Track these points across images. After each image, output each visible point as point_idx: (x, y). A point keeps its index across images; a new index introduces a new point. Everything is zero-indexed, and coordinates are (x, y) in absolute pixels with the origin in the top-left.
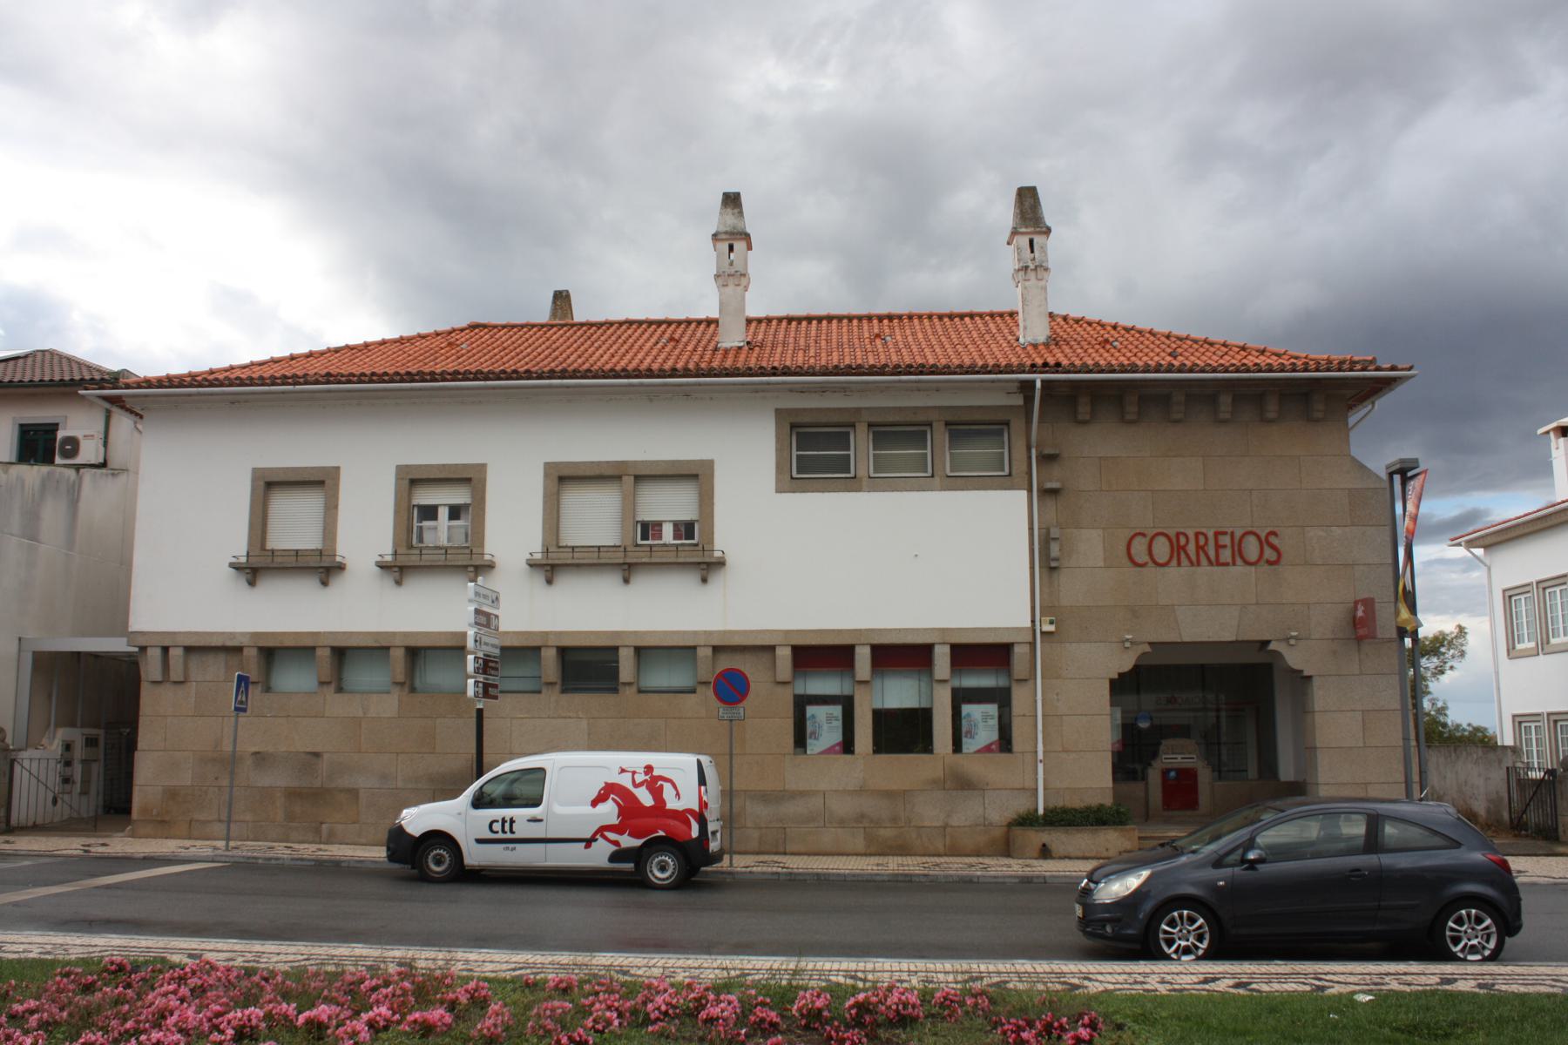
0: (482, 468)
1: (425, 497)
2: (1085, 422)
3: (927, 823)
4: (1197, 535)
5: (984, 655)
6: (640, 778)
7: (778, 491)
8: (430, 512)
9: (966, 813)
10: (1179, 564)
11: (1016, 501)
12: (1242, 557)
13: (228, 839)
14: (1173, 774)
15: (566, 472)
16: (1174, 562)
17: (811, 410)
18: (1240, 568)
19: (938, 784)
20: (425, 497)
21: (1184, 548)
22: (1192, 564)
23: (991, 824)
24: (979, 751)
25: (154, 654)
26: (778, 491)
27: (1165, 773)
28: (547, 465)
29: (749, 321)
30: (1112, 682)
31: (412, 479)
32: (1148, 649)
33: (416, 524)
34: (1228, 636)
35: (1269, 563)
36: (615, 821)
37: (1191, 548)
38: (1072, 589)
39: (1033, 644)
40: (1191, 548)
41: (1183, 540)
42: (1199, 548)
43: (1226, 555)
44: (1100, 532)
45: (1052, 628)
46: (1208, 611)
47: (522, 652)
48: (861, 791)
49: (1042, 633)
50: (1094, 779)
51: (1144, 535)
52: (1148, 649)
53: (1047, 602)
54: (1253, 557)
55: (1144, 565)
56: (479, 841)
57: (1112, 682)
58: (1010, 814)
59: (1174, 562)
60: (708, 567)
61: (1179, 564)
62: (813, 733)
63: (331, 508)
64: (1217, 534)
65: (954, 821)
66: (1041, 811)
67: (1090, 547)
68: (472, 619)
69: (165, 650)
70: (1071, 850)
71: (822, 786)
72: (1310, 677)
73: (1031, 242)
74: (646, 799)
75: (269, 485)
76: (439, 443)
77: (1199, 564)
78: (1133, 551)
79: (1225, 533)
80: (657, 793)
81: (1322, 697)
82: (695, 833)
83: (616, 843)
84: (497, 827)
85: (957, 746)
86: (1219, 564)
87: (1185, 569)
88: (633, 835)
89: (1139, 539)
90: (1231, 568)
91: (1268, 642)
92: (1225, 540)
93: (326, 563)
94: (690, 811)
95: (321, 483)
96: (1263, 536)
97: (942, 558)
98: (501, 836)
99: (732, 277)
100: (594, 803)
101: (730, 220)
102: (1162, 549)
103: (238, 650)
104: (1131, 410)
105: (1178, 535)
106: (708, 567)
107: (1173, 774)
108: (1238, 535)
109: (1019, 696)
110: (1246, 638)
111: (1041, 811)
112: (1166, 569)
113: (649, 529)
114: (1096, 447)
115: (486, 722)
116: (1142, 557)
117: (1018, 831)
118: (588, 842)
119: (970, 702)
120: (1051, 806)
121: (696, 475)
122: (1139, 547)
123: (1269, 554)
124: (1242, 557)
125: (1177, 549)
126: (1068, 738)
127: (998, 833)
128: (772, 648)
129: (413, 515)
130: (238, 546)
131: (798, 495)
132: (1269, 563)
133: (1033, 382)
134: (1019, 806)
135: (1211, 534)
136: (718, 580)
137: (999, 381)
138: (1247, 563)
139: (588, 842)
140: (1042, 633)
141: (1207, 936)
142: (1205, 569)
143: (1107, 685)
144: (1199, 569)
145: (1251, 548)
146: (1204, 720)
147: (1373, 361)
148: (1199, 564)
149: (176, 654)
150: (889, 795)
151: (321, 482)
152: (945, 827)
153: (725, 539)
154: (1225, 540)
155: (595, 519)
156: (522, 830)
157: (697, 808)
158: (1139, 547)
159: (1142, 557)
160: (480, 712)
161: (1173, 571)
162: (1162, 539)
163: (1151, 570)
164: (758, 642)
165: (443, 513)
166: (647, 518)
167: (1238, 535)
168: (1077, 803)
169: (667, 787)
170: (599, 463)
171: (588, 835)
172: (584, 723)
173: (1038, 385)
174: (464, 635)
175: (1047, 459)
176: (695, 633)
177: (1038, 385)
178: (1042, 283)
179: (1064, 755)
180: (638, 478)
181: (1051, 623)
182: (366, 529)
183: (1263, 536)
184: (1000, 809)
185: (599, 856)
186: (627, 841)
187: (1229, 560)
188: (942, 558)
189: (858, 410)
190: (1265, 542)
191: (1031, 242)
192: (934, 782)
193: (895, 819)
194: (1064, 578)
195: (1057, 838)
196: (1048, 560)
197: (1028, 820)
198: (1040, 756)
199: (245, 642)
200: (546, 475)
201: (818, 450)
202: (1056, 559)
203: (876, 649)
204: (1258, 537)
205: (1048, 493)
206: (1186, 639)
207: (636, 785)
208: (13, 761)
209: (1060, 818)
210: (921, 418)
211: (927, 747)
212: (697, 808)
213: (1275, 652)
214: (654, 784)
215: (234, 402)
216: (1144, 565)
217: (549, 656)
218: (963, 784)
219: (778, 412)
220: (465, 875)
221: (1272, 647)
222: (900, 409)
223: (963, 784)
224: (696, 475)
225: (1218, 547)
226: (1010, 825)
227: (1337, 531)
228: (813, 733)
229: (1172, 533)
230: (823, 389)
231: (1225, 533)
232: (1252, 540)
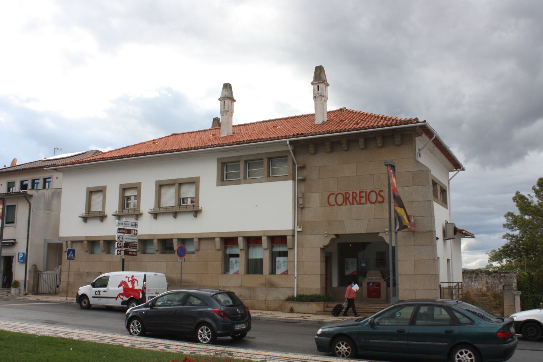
0: (140, 184)
1: (128, 193)
2: (399, 145)
3: (260, 299)
4: (353, 193)
5: (277, 240)
6: (130, 279)
7: (217, 186)
8: (129, 198)
9: (274, 295)
10: (346, 205)
11: (289, 184)
12: (369, 201)
13: (67, 297)
14: (371, 284)
15: (161, 184)
16: (345, 203)
17: (266, 153)
18: (369, 205)
19: (263, 285)
20: (128, 193)
21: (348, 198)
22: (351, 204)
24: (281, 274)
25: (64, 243)
26: (217, 186)
27: (369, 283)
28: (157, 182)
29: (233, 126)
31: (124, 189)
32: (334, 237)
33: (126, 202)
34: (363, 231)
35: (380, 202)
36: (122, 292)
38: (309, 215)
39: (293, 236)
41: (348, 195)
42: (354, 198)
43: (363, 200)
44: (319, 194)
45: (300, 230)
46: (358, 221)
47: (145, 243)
48: (241, 287)
49: (298, 232)
50: (314, 284)
51: (334, 194)
52: (334, 237)
53: (299, 220)
55: (333, 205)
56: (93, 297)
57: (321, 249)
58: (286, 297)
59: (345, 203)
60: (196, 212)
61: (346, 205)
62: (278, 267)
63: (104, 198)
64: (360, 192)
65: (268, 299)
66: (295, 296)
67: (315, 199)
68: (117, 231)
69: (67, 242)
70: (300, 310)
71: (229, 285)
73: (318, 86)
74: (130, 286)
75: (91, 192)
76: (129, 177)
77: (353, 204)
78: (330, 200)
79: (363, 192)
80: (133, 283)
81: (401, 255)
82: (141, 297)
83: (122, 299)
84: (97, 293)
85: (273, 271)
86: (361, 204)
87: (348, 206)
88: (127, 297)
89: (332, 196)
91: (379, 233)
92: (363, 194)
93: (101, 215)
94: (140, 290)
95: (102, 191)
97: (265, 206)
98: (97, 296)
99: (319, 97)
100: (119, 287)
101: (227, 94)
102: (340, 199)
103: (82, 242)
104: (398, 140)
105: (346, 193)
106: (196, 212)
107: (371, 284)
110: (370, 232)
111: (295, 296)
112: (341, 206)
113: (184, 200)
114: (320, 162)
115: (125, 263)
116: (333, 203)
118: (116, 298)
119: (280, 256)
120: (299, 294)
121: (194, 182)
122: (332, 198)
123: (380, 199)
124: (369, 201)
126: (304, 270)
128: (214, 238)
129: (124, 201)
130: (82, 210)
131: (231, 186)
132: (380, 202)
133: (286, 141)
134: (288, 294)
135: (358, 193)
136: (200, 216)
137: (281, 142)
138: (371, 203)
139: (116, 298)
140: (298, 232)
141: (460, 351)
142: (356, 206)
143: (319, 250)
145: (373, 197)
146: (358, 262)
147: (417, 119)
148: (353, 204)
149: (69, 243)
150: (249, 288)
151: (101, 190)
152: (266, 300)
153: (202, 204)
154: (363, 194)
155: (169, 198)
156: (103, 294)
157: (142, 289)
159: (333, 203)
160: (123, 260)
161: (344, 207)
162: (340, 195)
163: (336, 207)
164: (210, 237)
165: (132, 198)
166: (183, 197)
167: (368, 192)
168: (308, 293)
169: (136, 282)
170: (169, 180)
171: (116, 296)
172: (165, 264)
173: (288, 142)
174: (115, 236)
175: (301, 168)
176: (193, 234)
180: (180, 184)
181: (300, 228)
182: (112, 205)
183: (377, 192)
184: (283, 295)
185: (118, 303)
186: (125, 299)
187: (365, 202)
188: (265, 206)
189: (241, 156)
191: (318, 86)
192: (263, 284)
193: (250, 297)
194: (306, 211)
195: (296, 306)
196: (300, 205)
197: (291, 299)
198: (296, 276)
199: (84, 239)
200: (156, 185)
201: (228, 172)
203: (221, 238)
204: (375, 192)
206: (348, 233)
207: (129, 281)
208: (39, 274)
209: (301, 299)
210: (260, 157)
211: (261, 273)
212: (142, 289)
214: (133, 281)
215: (82, 168)
216: (333, 205)
217: (218, 240)
218: (272, 285)
219: (218, 159)
220: (89, 307)
221: (380, 235)
222: (253, 155)
223: (272, 285)
224: (194, 182)
225: (361, 197)
227: (407, 189)
228: (278, 267)
229: (344, 193)
230: (228, 150)
231: (363, 192)
232: (373, 193)
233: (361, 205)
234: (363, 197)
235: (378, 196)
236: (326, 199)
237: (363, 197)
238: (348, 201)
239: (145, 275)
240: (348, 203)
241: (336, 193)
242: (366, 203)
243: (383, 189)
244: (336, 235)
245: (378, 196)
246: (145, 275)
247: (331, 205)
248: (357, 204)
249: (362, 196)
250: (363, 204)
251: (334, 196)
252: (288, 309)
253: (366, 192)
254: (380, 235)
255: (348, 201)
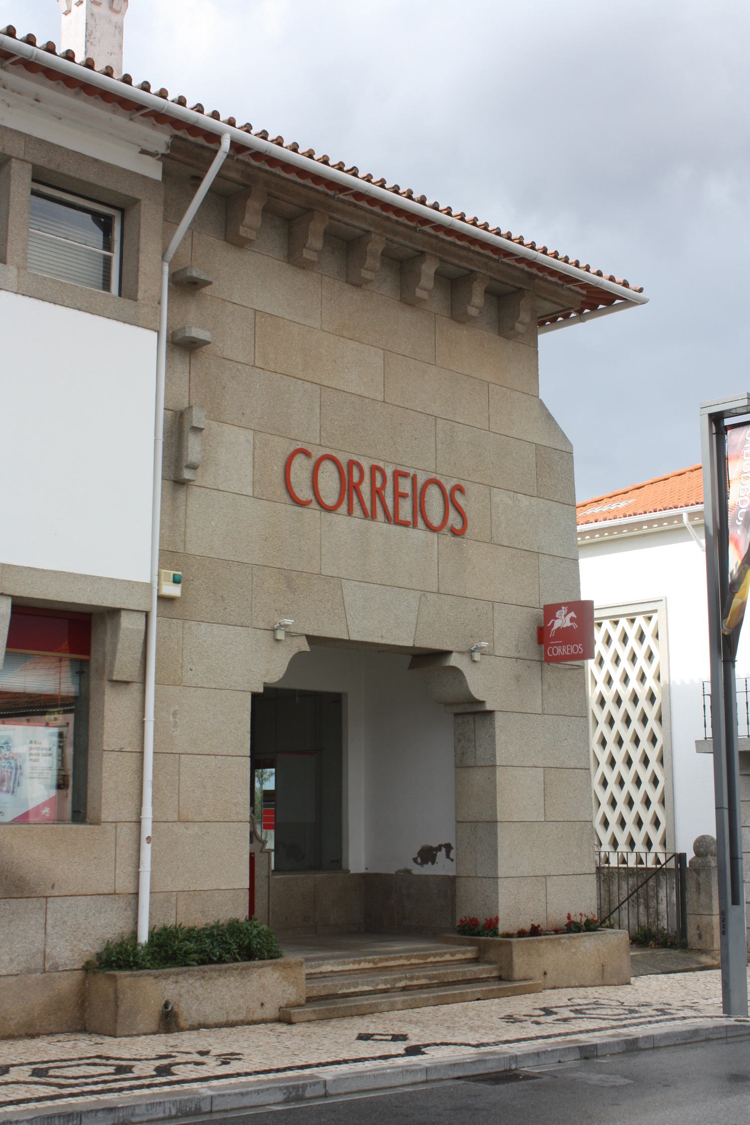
10: (350, 512)
12: (424, 517)
16: (344, 508)
18: (419, 534)
23: (55, 968)
30: (255, 696)
32: (306, 647)
35: (455, 533)
37: (365, 488)
40: (365, 488)
42: (376, 492)
43: (406, 509)
44: (250, 435)
51: (307, 454)
54: (436, 519)
57: (255, 696)
58: (89, 947)
59: (344, 508)
61: (350, 512)
64: (397, 474)
72: (491, 712)
77: (374, 517)
79: (405, 475)
87: (357, 522)
90: (410, 531)
91: (449, 653)
92: (405, 486)
96: (448, 488)
108: (421, 481)
109: (114, 712)
111: (143, 937)
114: (256, 288)
116: (305, 494)
117: (101, 984)
122: (301, 470)
123: (454, 519)
124: (424, 517)
125: (349, 488)
127: (66, 984)
134: (102, 927)
135: (389, 472)
142: (379, 526)
144: (372, 524)
148: (374, 517)
154: (405, 486)
158: (301, 470)
159: (305, 494)
161: (340, 519)
163: (313, 513)
167: (421, 481)
173: (226, 144)
177: (226, 144)
178: (115, 18)
179: (180, 828)
181: (176, 581)
183: (448, 488)
184: (73, 934)
187: (409, 518)
190: (449, 501)
194: (195, 501)
197: (118, 958)
202: (193, 467)
205: (182, 346)
206: (355, 637)
209: (174, 949)
213: (455, 669)
225: (398, 495)
226: (88, 968)
227: (524, 501)
229: (343, 459)
231: (405, 475)
232: (433, 491)
233: (394, 528)
234: (404, 496)
235: (451, 507)
236: (278, 469)
237: (404, 496)
238: (355, 500)
239: (311, 501)
240: (357, 511)
241: (317, 453)
242: (415, 525)
243: (462, 483)
244: (311, 639)
245: (451, 507)
246: (311, 501)
247: (297, 502)
248: (388, 519)
249: (401, 490)
250: (405, 524)
251: (309, 464)
252: (150, 1015)
253: (414, 479)
254: (454, 661)
255: (355, 500)
